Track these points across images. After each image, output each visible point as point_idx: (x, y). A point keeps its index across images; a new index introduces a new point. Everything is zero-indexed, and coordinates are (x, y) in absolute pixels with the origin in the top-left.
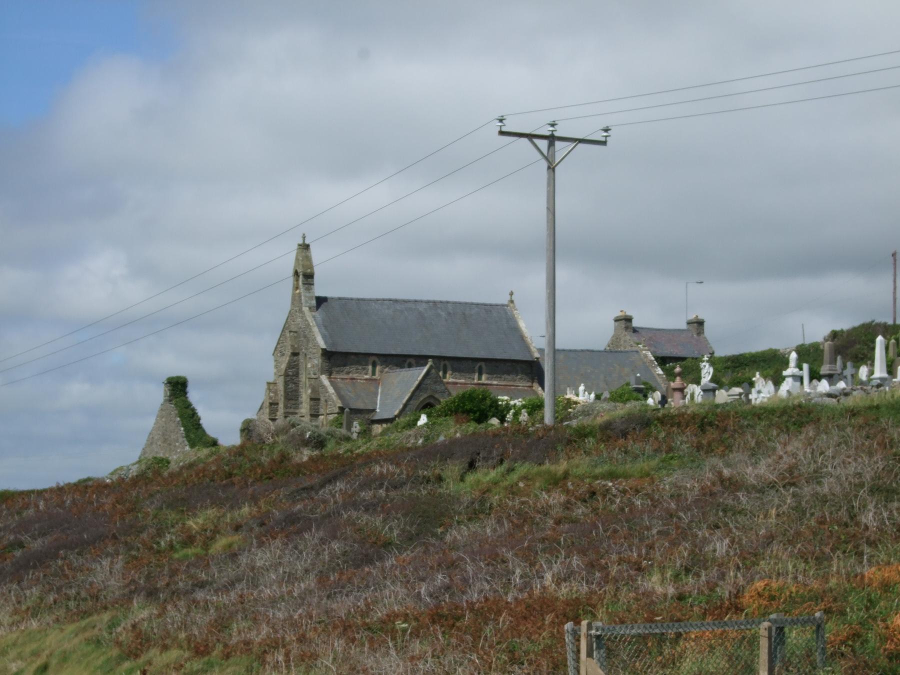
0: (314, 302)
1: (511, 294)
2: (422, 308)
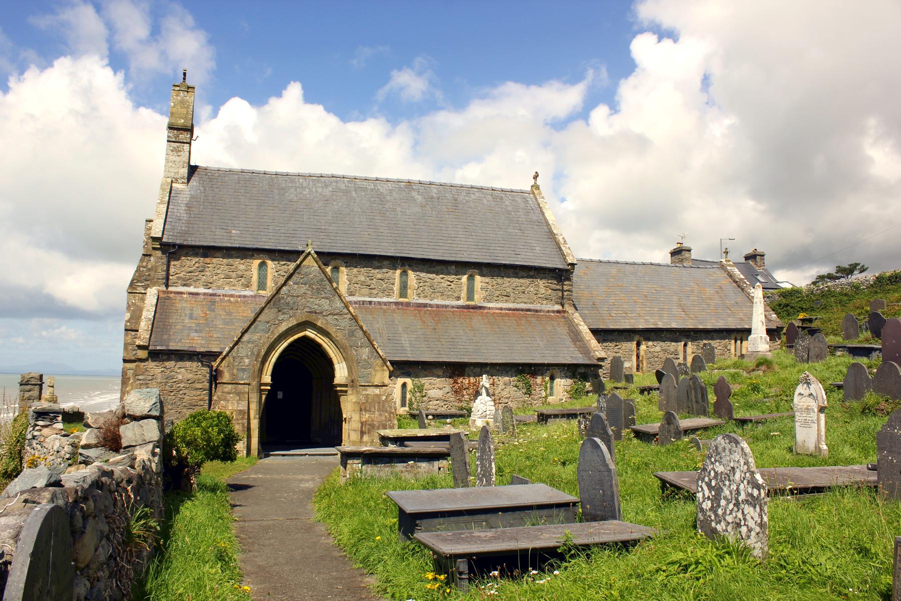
0: (184, 171)
1: (536, 177)
2: (383, 188)
